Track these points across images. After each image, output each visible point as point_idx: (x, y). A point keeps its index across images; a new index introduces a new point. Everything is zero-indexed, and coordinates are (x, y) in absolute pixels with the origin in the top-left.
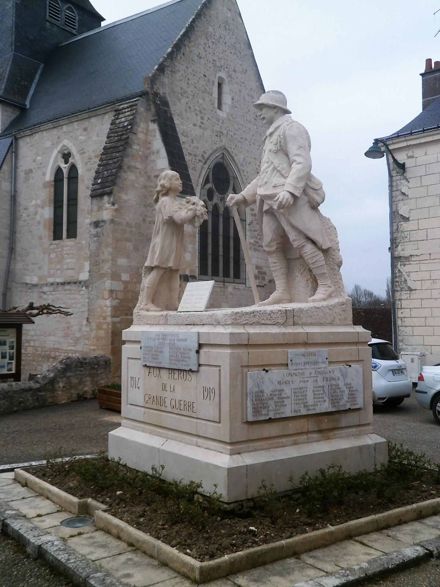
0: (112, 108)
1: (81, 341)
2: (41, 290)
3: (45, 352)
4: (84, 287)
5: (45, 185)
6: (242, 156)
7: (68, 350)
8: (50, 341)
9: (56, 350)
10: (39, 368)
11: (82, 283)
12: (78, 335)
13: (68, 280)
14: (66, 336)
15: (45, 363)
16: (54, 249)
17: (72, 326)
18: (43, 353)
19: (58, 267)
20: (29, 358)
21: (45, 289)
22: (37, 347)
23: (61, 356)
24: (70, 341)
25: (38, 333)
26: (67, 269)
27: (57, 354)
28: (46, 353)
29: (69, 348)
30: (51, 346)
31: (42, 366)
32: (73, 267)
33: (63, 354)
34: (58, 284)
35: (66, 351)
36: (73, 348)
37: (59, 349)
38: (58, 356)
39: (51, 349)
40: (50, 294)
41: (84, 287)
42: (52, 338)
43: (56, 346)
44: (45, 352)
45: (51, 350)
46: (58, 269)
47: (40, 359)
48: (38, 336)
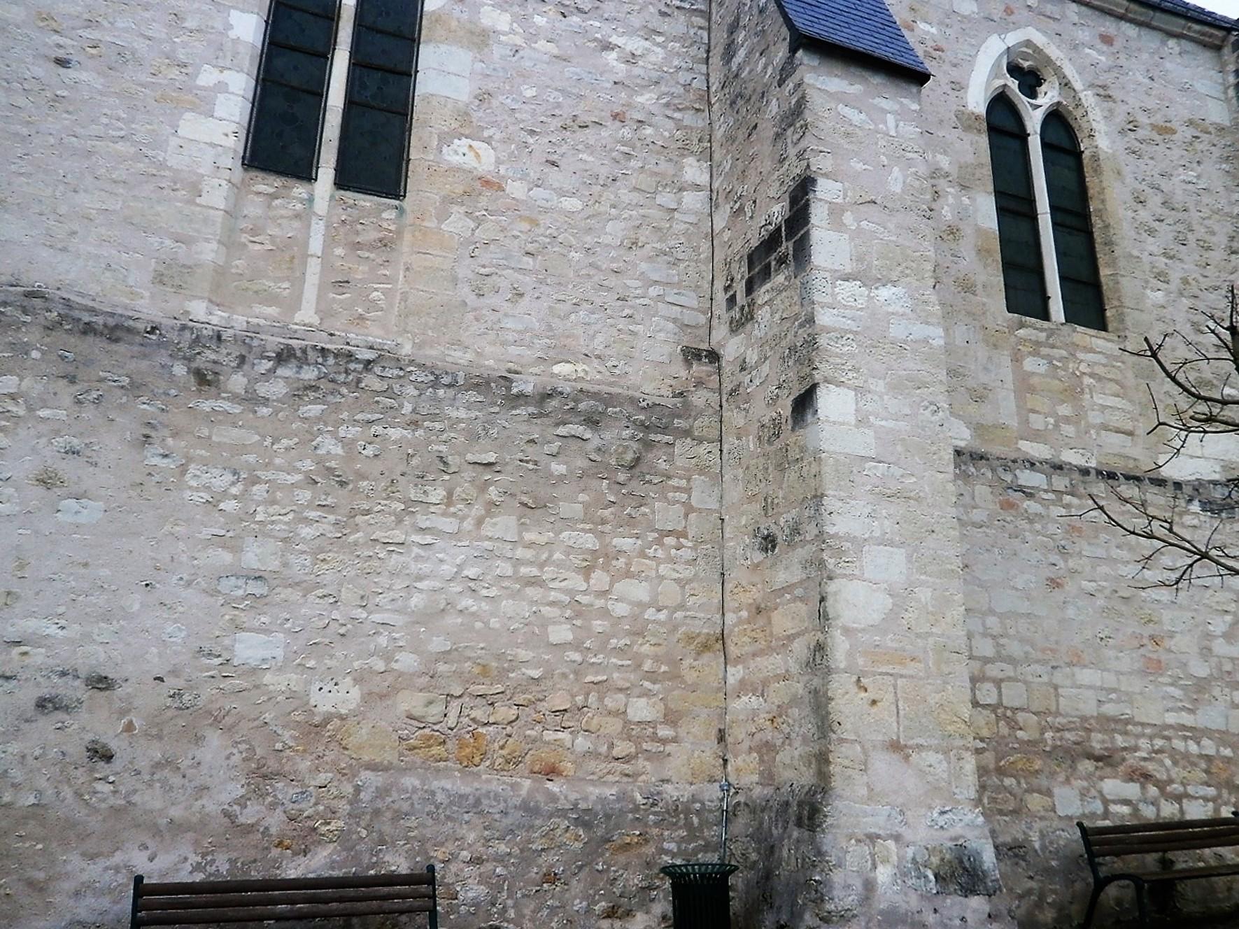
0: (1203, 34)
1: (1216, 692)
2: (1008, 478)
3: (1058, 730)
4: (1196, 503)
5: (965, 120)
6: (277, 562)
7: (1170, 727)
8: (1080, 687)
9: (1110, 723)
10: (1035, 802)
11: (1188, 490)
12: (1201, 670)
13: (1119, 466)
14: (1153, 668)
15: (1061, 778)
16: (1038, 343)
17: (1171, 635)
18: (1048, 735)
19: (1065, 410)
20: (1100, 736)
21: (1028, 478)
22: (1015, 710)
23: (1136, 749)
24: (1172, 690)
25: (1015, 649)
26: (1105, 427)
27: (1120, 741)
28: (1067, 735)
29: (1171, 718)
30: (1090, 709)
31: (1049, 793)
32: (1129, 426)
33: (1143, 743)
34: (1085, 472)
35: (1161, 730)
36: (1187, 719)
37: (1127, 722)
38: (1125, 749)
39: (1084, 719)
40: (1053, 503)
41: (1196, 503)
42: (1086, 676)
43: (1110, 709)
44: (1058, 730)
45: (1085, 723)
46: (1067, 420)
47: (1038, 764)
48: (1011, 660)
